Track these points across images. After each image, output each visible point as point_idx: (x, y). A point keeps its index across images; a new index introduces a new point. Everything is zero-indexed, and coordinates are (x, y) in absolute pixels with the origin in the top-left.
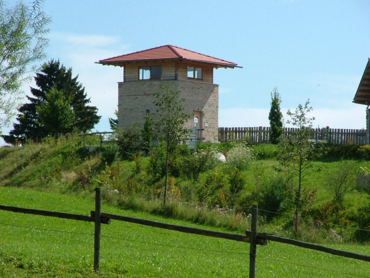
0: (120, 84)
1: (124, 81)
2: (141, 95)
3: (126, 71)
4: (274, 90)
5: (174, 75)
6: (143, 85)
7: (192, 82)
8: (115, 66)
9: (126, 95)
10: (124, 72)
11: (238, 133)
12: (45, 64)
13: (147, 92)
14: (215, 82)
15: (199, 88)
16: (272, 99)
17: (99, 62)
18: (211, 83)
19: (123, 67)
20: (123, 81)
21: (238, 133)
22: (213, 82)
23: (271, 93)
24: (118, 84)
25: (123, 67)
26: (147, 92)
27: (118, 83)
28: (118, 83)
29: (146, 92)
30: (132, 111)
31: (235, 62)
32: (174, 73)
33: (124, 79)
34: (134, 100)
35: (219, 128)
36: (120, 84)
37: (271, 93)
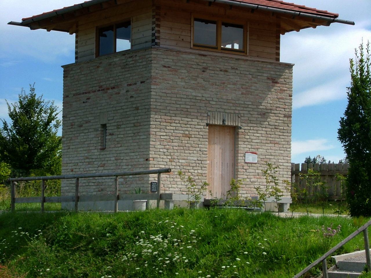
0: (67, 69)
1: (76, 62)
2: (95, 91)
3: (79, 39)
4: (359, 52)
5: (150, 38)
6: (98, 67)
7: (204, 55)
8: (49, 30)
9: (74, 92)
10: (77, 42)
11: (300, 170)
12: (346, 111)
13: (104, 83)
14: (283, 59)
15: (226, 71)
16: (353, 77)
17: (21, 21)
18: (274, 61)
19: (74, 34)
20: (73, 61)
21: (300, 170)
22: (278, 59)
23: (351, 61)
24: (62, 69)
25: (74, 34)
26: (104, 83)
27: (62, 67)
28: (62, 67)
29: (101, 84)
30: (82, 128)
31: (331, 10)
32: (150, 32)
33: (76, 58)
34: (84, 105)
35: (292, 164)
36: (67, 69)
37: (351, 61)
